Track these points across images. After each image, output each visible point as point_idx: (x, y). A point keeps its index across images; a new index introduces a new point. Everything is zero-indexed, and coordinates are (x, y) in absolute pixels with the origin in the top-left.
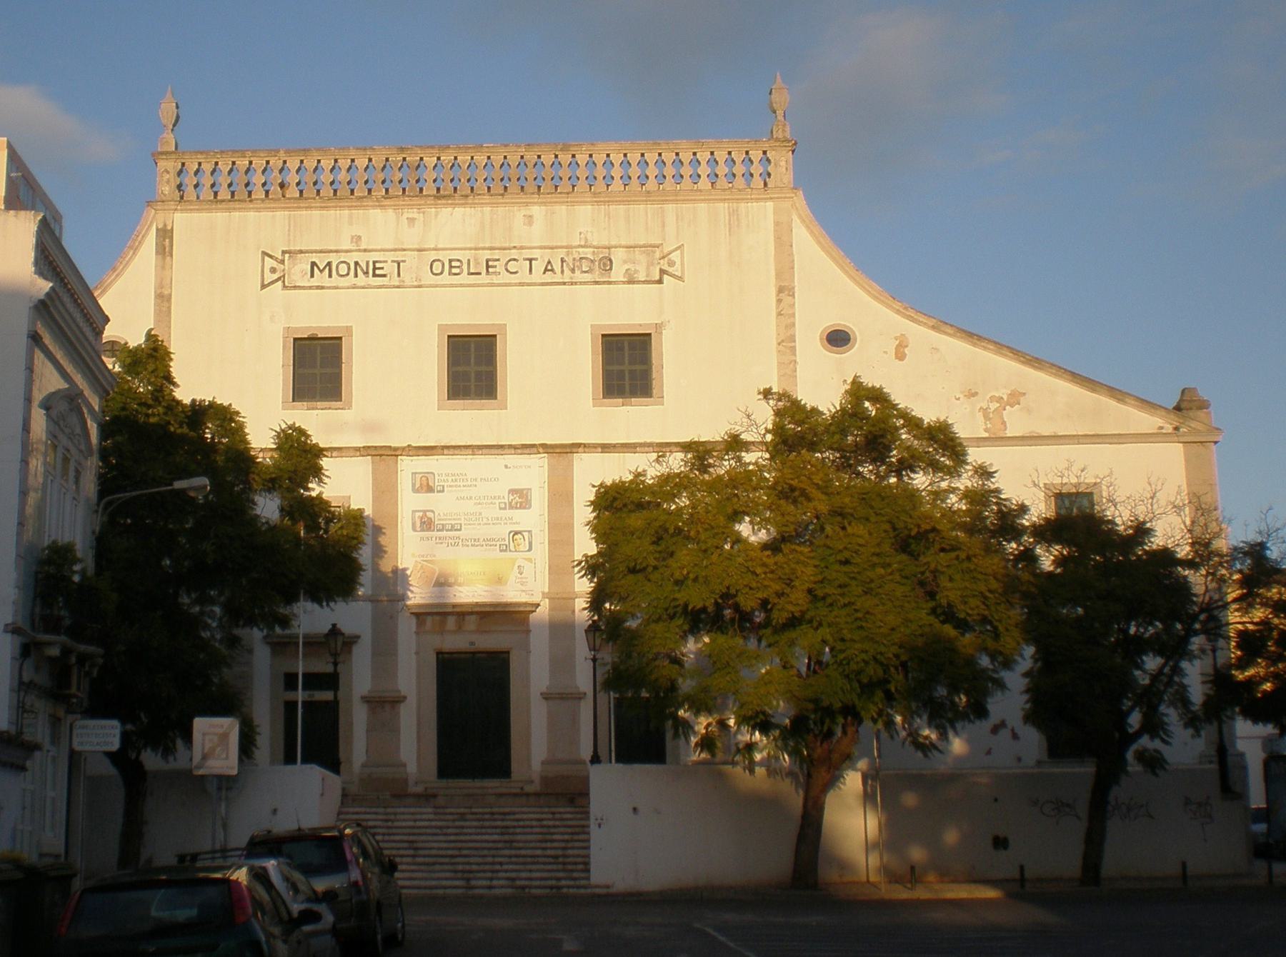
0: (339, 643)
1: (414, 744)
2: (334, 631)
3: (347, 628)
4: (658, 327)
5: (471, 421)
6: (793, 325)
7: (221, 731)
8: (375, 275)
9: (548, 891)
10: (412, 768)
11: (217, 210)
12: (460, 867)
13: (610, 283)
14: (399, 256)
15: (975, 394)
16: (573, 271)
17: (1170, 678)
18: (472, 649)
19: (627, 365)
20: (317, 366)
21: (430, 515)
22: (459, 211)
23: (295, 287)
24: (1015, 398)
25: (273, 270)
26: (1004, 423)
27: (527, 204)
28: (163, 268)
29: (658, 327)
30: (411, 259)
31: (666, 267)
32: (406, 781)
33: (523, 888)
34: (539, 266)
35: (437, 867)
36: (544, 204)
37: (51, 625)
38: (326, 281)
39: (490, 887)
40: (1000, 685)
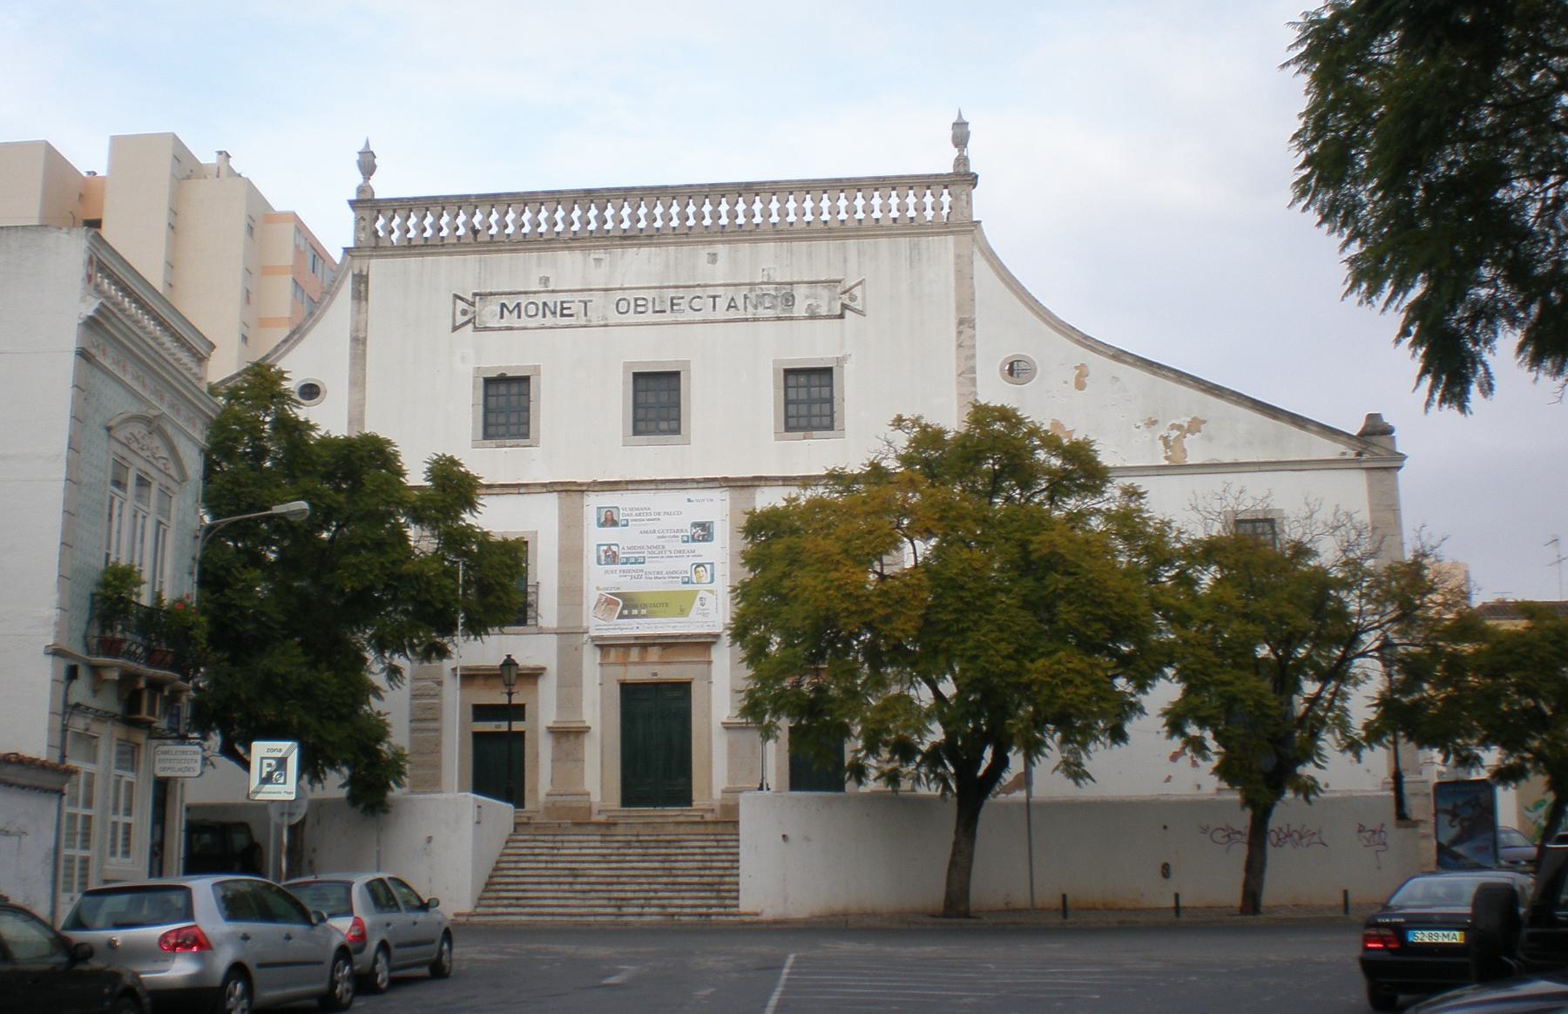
0: (513, 676)
1: (597, 775)
2: (509, 663)
3: (525, 660)
4: (841, 361)
5: (654, 458)
6: (973, 356)
7: (280, 755)
8: (562, 315)
9: (696, 919)
10: (596, 798)
11: (411, 255)
12: (615, 895)
13: (791, 319)
14: (586, 296)
15: (1155, 423)
16: (756, 307)
17: (1331, 702)
18: (654, 679)
19: (809, 396)
20: (506, 404)
21: (614, 548)
22: (645, 251)
23: (486, 329)
24: (1195, 425)
25: (464, 313)
26: (1184, 450)
27: (711, 243)
28: (359, 312)
29: (841, 361)
30: (597, 299)
31: (847, 302)
32: (589, 809)
33: (673, 915)
34: (722, 303)
35: (593, 894)
36: (729, 242)
37: (110, 647)
38: (516, 323)
39: (640, 915)
40: (1137, 709)
